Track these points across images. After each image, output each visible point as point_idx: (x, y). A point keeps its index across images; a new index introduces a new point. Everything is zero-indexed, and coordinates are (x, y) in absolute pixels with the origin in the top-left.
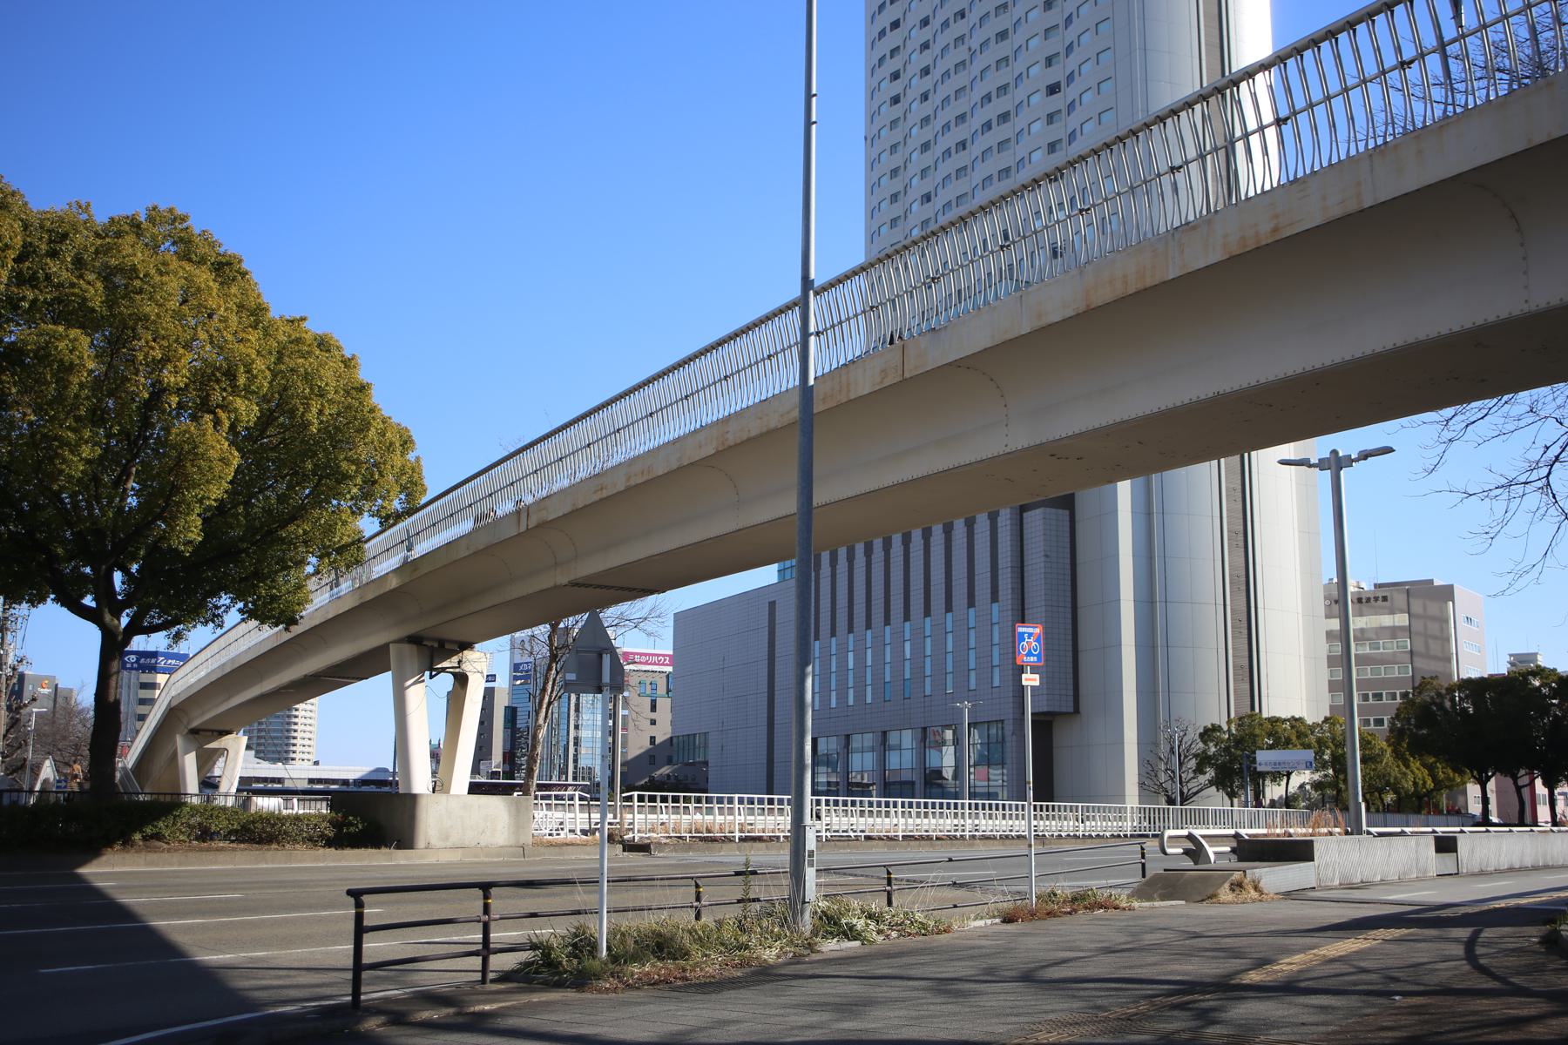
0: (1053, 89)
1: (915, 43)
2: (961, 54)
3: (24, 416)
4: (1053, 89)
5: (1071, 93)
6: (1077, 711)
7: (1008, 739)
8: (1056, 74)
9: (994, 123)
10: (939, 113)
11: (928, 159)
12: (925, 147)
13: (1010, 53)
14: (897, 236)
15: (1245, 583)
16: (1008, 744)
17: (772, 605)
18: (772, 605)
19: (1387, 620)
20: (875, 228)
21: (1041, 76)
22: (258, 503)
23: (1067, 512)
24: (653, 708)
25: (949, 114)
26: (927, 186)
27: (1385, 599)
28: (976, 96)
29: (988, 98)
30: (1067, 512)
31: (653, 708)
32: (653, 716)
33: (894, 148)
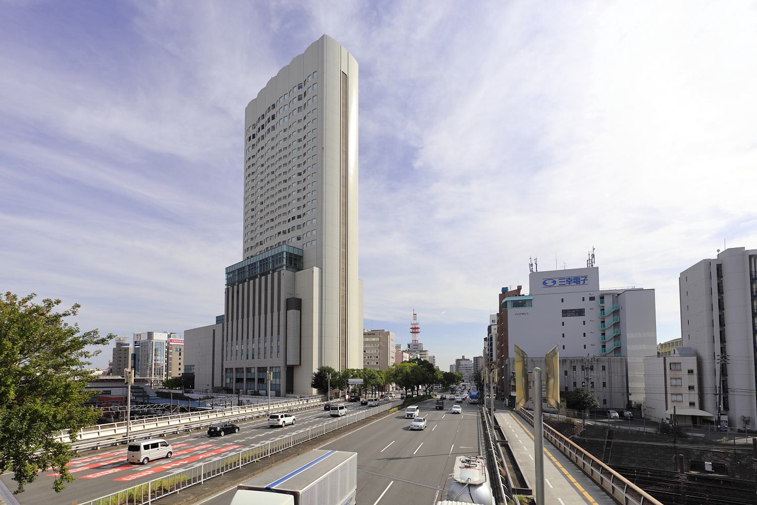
0: (300, 174)
1: (259, 164)
2: (273, 177)
3: (3, 388)
4: (300, 174)
5: (304, 176)
6: (300, 364)
7: (281, 372)
8: (301, 170)
9: (282, 199)
10: (266, 224)
11: (262, 207)
12: (262, 180)
13: (287, 170)
14: (253, 243)
15: (344, 320)
16: (281, 373)
17: (214, 330)
18: (214, 330)
19: (374, 339)
20: (247, 182)
21: (296, 170)
22: (68, 380)
23: (299, 311)
24: (180, 355)
25: (269, 171)
26: (262, 200)
27: (374, 334)
28: (277, 190)
29: (280, 191)
30: (299, 311)
31: (180, 355)
32: (180, 357)
33: (252, 217)
